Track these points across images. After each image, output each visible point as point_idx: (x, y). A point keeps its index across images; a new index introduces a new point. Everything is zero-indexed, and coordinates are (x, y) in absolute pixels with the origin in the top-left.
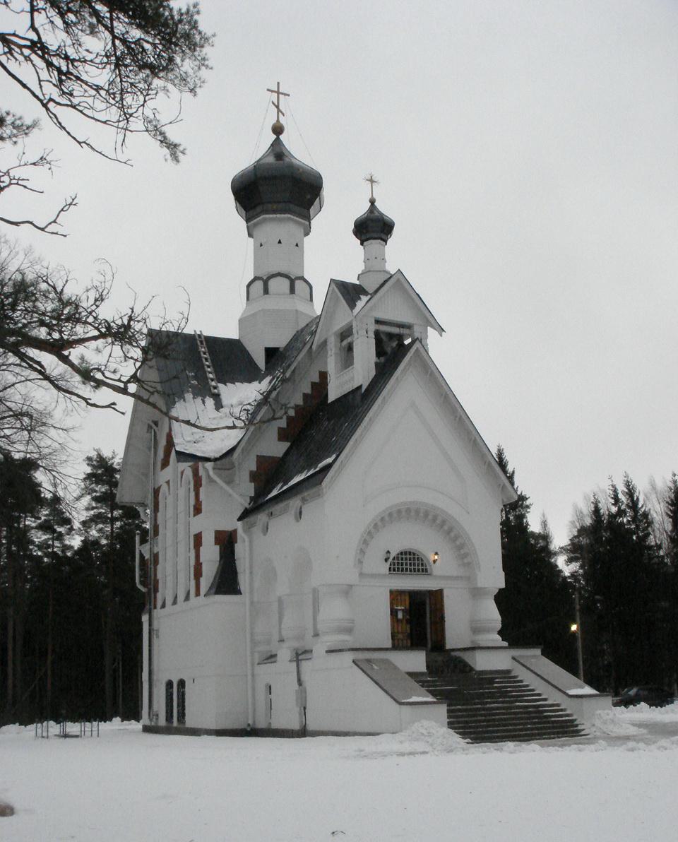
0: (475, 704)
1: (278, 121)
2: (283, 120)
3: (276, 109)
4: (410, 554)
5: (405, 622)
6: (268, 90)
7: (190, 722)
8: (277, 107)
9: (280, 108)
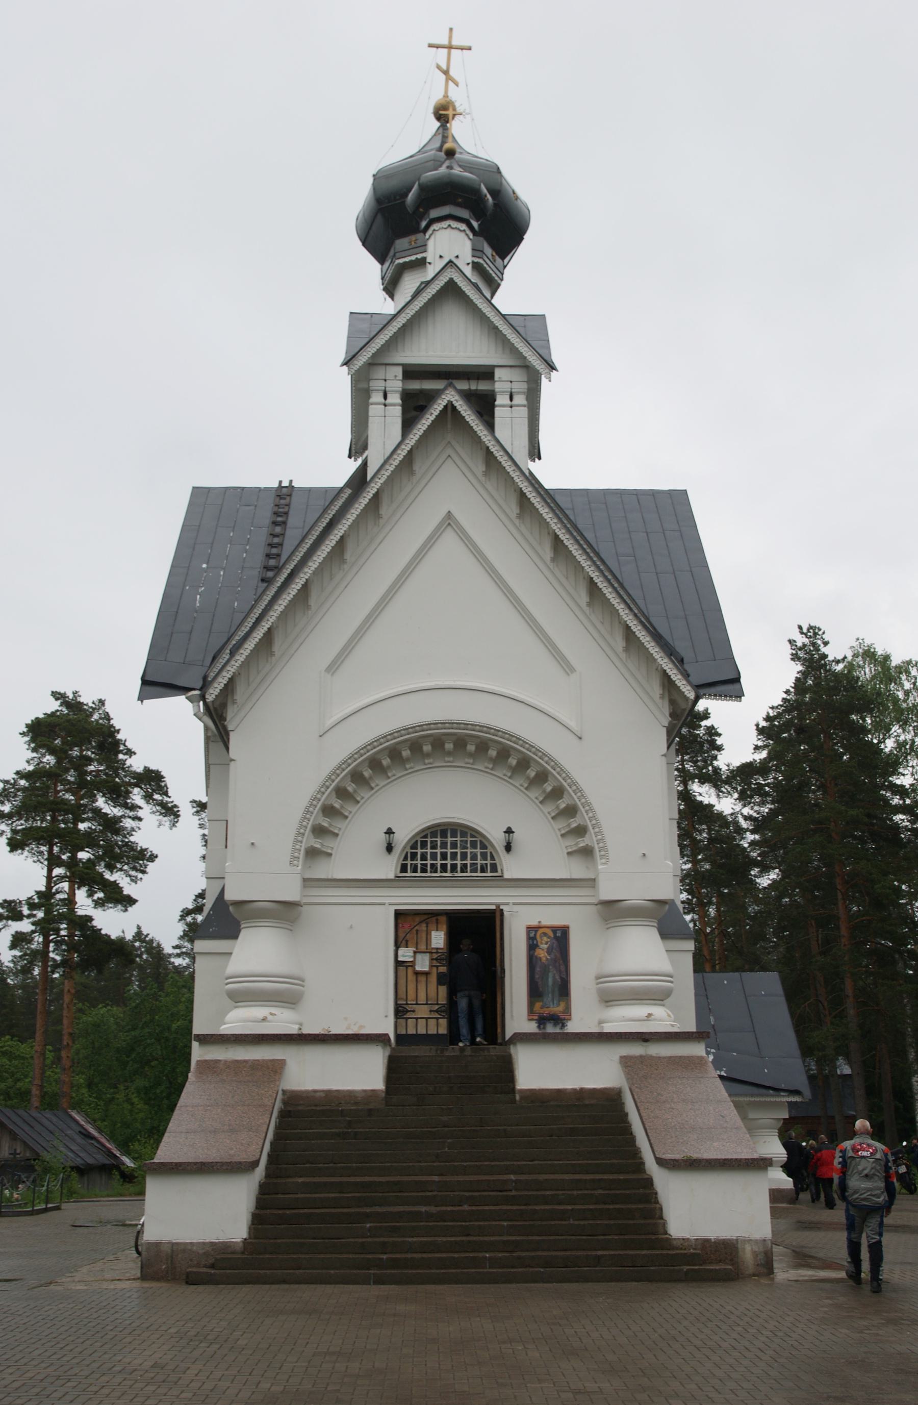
0: (563, 1194)
1: (446, 96)
2: (455, 95)
3: (443, 77)
4: (454, 835)
5: (433, 978)
6: (430, 46)
7: (398, 1020)
8: (446, 72)
9: (452, 73)
